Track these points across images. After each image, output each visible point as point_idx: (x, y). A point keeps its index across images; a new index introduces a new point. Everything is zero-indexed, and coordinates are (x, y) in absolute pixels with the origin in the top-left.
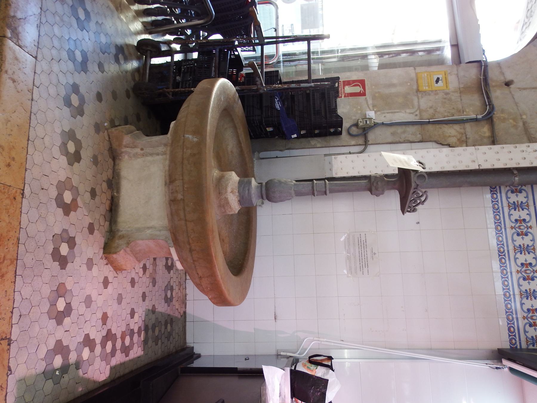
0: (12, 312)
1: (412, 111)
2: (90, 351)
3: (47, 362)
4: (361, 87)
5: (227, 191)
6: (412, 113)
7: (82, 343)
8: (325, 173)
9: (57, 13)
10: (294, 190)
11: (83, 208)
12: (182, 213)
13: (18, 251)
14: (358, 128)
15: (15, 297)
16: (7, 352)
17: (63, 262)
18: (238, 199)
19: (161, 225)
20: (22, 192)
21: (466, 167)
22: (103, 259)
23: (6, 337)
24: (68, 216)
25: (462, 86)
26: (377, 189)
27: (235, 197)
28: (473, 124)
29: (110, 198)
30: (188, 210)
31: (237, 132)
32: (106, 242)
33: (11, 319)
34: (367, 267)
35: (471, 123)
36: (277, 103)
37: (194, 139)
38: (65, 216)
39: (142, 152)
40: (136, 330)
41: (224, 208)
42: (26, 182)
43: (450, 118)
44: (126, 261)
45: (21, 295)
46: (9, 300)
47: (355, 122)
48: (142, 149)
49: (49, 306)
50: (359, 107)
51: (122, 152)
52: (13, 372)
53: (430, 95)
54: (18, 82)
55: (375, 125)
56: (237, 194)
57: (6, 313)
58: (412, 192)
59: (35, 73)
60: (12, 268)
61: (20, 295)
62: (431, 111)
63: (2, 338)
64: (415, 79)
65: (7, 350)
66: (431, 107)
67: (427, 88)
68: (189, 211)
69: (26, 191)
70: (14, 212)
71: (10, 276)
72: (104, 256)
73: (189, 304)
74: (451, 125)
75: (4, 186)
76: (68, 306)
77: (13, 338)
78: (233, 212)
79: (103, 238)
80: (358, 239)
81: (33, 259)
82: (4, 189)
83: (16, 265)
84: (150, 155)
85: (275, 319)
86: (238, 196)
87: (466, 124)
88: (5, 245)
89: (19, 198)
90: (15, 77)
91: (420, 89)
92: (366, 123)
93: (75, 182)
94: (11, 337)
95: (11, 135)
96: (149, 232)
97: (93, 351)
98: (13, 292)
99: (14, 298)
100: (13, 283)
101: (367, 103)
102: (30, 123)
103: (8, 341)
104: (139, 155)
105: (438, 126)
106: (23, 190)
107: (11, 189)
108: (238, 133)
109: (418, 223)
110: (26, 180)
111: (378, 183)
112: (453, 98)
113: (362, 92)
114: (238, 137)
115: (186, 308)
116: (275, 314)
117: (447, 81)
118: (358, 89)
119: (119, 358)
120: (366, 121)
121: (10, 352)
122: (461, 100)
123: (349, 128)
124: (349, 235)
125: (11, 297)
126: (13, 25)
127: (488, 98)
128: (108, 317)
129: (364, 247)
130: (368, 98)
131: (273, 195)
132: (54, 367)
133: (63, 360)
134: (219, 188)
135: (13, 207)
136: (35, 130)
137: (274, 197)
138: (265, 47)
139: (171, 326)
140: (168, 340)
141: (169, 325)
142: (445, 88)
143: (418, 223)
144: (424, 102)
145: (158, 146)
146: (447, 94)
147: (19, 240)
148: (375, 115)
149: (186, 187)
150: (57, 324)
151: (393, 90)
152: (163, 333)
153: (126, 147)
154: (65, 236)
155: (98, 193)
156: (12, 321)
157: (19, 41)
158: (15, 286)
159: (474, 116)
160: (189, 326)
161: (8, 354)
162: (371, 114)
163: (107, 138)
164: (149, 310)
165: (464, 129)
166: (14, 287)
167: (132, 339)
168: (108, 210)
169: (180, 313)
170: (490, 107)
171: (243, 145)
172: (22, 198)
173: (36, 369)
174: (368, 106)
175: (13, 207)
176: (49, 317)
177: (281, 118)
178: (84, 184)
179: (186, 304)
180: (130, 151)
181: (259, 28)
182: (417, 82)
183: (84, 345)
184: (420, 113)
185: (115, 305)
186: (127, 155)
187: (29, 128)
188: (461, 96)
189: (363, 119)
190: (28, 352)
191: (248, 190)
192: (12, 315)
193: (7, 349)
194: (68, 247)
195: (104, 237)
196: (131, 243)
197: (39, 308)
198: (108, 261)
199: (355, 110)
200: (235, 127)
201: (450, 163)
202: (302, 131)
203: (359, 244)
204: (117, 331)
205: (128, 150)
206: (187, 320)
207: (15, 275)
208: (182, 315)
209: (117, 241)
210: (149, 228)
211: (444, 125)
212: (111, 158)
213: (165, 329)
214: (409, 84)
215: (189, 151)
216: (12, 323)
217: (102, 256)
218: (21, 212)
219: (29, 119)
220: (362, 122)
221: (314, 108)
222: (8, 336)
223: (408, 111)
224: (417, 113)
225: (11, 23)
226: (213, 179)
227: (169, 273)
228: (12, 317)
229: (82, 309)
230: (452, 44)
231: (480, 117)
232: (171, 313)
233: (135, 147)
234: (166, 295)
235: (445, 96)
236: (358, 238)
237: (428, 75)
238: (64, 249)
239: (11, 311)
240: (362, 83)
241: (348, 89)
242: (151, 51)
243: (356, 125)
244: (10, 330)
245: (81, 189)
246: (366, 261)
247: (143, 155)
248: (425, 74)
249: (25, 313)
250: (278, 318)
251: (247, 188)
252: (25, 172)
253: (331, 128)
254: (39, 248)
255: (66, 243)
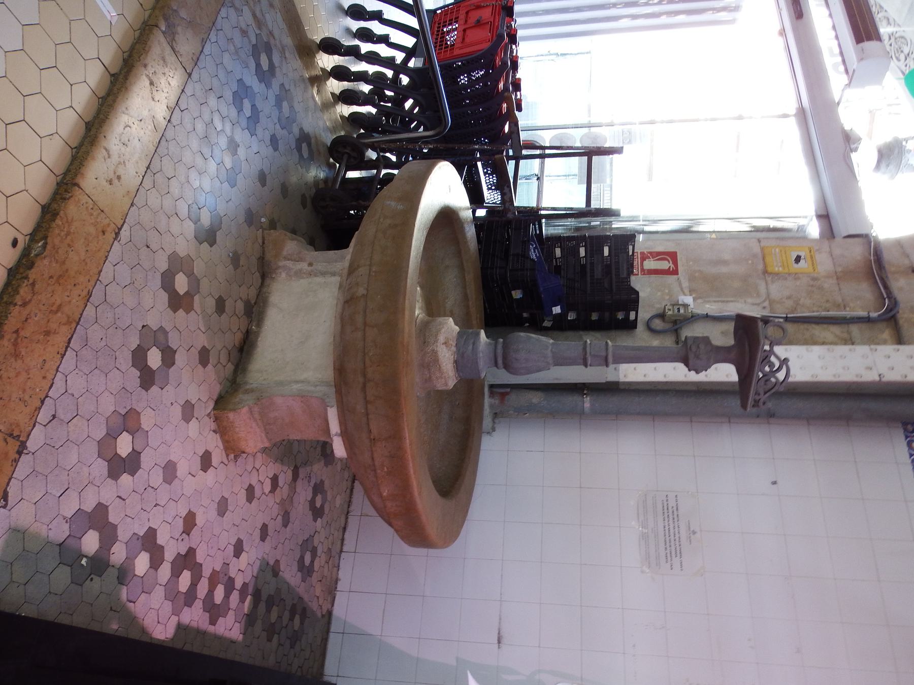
0: (43, 402)
1: (758, 301)
2: (151, 564)
3: (71, 529)
4: (671, 262)
5: (438, 340)
6: (758, 304)
7: (140, 538)
8: (606, 373)
9: (232, 40)
10: (551, 351)
11: (200, 316)
12: (359, 319)
13: (83, 311)
14: (664, 321)
15: (55, 380)
16: (11, 464)
17: (148, 379)
18: (454, 357)
19: (320, 379)
20: (117, 231)
21: (857, 376)
22: (210, 418)
23: (19, 436)
24: (175, 313)
25: (839, 269)
26: (697, 357)
27: (450, 353)
28: (864, 326)
29: (244, 330)
30: (371, 307)
31: (464, 277)
32: (222, 395)
33: (37, 412)
34: (679, 555)
35: (860, 325)
36: (532, 250)
37: (399, 206)
38: (169, 309)
39: (310, 268)
40: (238, 584)
41: (429, 369)
42: (127, 220)
43: (824, 314)
44: (248, 432)
45: (66, 384)
46: (44, 378)
47: (661, 311)
48: (310, 264)
49: (104, 433)
50: (667, 291)
51: (279, 267)
52: (8, 507)
53: (786, 279)
54: (156, 87)
55: (692, 317)
56: (454, 349)
57: (32, 396)
58: (760, 359)
59: (183, 91)
60: (65, 330)
61: (65, 383)
62: (789, 303)
63: (12, 433)
64: (760, 256)
65: (12, 461)
66: (789, 298)
67: (781, 269)
68: (372, 309)
69: (122, 232)
70: (95, 250)
71: (59, 340)
72: (214, 414)
73: (340, 599)
74: (825, 326)
75: (94, 205)
76: (135, 455)
77: (31, 445)
78: (443, 380)
79: (219, 386)
80: (663, 503)
81: (102, 339)
82: (92, 209)
83: (73, 329)
84: (322, 274)
85: (499, 642)
86: (455, 352)
87: (850, 325)
88: (67, 289)
89: (110, 236)
90: (154, 79)
91: (770, 269)
92: (679, 311)
93: (199, 268)
94: (27, 441)
95: (126, 145)
96: (296, 387)
97: (156, 570)
98: (55, 369)
99: (53, 379)
100: (59, 356)
101: (680, 285)
102: (157, 147)
103: (19, 446)
104: (304, 273)
105: (802, 327)
106: (120, 229)
107: (102, 215)
108: (465, 280)
109: (774, 483)
110: (127, 217)
111: (700, 346)
112: (826, 286)
113: (671, 269)
114: (464, 287)
115: (333, 605)
116: (499, 633)
117: (814, 261)
118: (665, 265)
119: (194, 616)
120: (679, 309)
121: (16, 466)
122: (840, 289)
123: (649, 320)
124: (646, 495)
125: (50, 377)
126: (172, 19)
127: (886, 287)
128: (196, 525)
129: (674, 519)
130: (682, 279)
131: (514, 356)
132: (81, 547)
133: (100, 547)
134: (425, 335)
135: (98, 243)
136: (161, 161)
137: (516, 360)
138: (522, 162)
139: (302, 623)
140: (292, 647)
141: (297, 618)
142: (811, 270)
143: (774, 483)
144: (777, 290)
145: (336, 261)
146: (814, 279)
147: (90, 296)
148: (694, 304)
149: (374, 270)
150: (109, 473)
151: (724, 269)
152: (284, 625)
153: (286, 259)
154: (161, 337)
155: (227, 309)
156: (37, 416)
157: (174, 42)
158: (61, 362)
159: (863, 314)
160: (334, 640)
161: (12, 469)
162: (688, 300)
163: (260, 241)
164: (268, 563)
165: (849, 333)
166: (59, 362)
167: (227, 596)
168: (237, 346)
169: (321, 608)
170: (889, 301)
171: (470, 303)
172: (115, 239)
173: (50, 529)
174: (682, 289)
175: (98, 243)
176: (99, 451)
177: (537, 272)
178: (211, 282)
179: (335, 597)
180: (291, 266)
181: (516, 128)
182: (764, 259)
183: (143, 545)
184: (770, 304)
185: (213, 513)
186: (286, 272)
187: (154, 154)
188: (838, 284)
189: (673, 305)
190: (45, 488)
191: (474, 344)
192: (41, 406)
193: (14, 458)
194: (161, 359)
195: (220, 384)
196: (262, 399)
197: (88, 425)
198: (219, 427)
199: (659, 294)
200: (461, 268)
201: (826, 369)
202: (569, 314)
203: (664, 513)
204: (204, 557)
205: (289, 263)
206: (332, 629)
207: (66, 345)
208: (324, 613)
209: (241, 396)
210: (297, 382)
211: (814, 326)
212: (259, 272)
213: (290, 620)
214: (750, 262)
215: (388, 221)
216: (36, 419)
217: (210, 413)
218: (107, 257)
219: (158, 141)
220: (672, 310)
221: (592, 276)
222: (23, 437)
223: (750, 300)
224: (766, 304)
225: (170, 16)
226: (417, 321)
227: (315, 520)
228: (40, 408)
229: (157, 478)
230: (819, 213)
231: (874, 315)
232: (306, 598)
233: (301, 260)
234: (302, 558)
235: (812, 283)
236: (663, 501)
237: (781, 251)
238: (154, 359)
239: (41, 399)
240: (673, 256)
241: (650, 264)
242: (350, 156)
243: (662, 316)
244: (30, 428)
245: (205, 285)
246: (678, 545)
247: (310, 274)
248: (777, 250)
249: (62, 417)
250: (504, 641)
251: (472, 341)
252: (130, 207)
253: (619, 311)
254: (116, 328)
255: (160, 350)
